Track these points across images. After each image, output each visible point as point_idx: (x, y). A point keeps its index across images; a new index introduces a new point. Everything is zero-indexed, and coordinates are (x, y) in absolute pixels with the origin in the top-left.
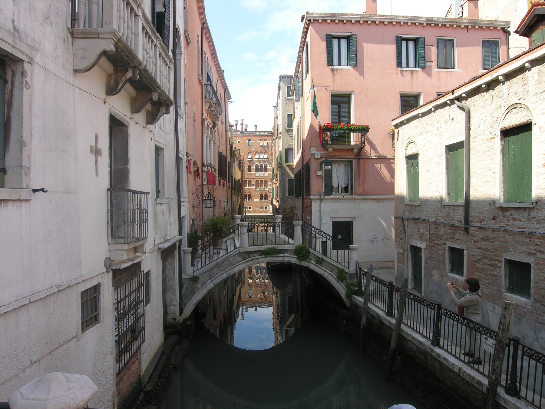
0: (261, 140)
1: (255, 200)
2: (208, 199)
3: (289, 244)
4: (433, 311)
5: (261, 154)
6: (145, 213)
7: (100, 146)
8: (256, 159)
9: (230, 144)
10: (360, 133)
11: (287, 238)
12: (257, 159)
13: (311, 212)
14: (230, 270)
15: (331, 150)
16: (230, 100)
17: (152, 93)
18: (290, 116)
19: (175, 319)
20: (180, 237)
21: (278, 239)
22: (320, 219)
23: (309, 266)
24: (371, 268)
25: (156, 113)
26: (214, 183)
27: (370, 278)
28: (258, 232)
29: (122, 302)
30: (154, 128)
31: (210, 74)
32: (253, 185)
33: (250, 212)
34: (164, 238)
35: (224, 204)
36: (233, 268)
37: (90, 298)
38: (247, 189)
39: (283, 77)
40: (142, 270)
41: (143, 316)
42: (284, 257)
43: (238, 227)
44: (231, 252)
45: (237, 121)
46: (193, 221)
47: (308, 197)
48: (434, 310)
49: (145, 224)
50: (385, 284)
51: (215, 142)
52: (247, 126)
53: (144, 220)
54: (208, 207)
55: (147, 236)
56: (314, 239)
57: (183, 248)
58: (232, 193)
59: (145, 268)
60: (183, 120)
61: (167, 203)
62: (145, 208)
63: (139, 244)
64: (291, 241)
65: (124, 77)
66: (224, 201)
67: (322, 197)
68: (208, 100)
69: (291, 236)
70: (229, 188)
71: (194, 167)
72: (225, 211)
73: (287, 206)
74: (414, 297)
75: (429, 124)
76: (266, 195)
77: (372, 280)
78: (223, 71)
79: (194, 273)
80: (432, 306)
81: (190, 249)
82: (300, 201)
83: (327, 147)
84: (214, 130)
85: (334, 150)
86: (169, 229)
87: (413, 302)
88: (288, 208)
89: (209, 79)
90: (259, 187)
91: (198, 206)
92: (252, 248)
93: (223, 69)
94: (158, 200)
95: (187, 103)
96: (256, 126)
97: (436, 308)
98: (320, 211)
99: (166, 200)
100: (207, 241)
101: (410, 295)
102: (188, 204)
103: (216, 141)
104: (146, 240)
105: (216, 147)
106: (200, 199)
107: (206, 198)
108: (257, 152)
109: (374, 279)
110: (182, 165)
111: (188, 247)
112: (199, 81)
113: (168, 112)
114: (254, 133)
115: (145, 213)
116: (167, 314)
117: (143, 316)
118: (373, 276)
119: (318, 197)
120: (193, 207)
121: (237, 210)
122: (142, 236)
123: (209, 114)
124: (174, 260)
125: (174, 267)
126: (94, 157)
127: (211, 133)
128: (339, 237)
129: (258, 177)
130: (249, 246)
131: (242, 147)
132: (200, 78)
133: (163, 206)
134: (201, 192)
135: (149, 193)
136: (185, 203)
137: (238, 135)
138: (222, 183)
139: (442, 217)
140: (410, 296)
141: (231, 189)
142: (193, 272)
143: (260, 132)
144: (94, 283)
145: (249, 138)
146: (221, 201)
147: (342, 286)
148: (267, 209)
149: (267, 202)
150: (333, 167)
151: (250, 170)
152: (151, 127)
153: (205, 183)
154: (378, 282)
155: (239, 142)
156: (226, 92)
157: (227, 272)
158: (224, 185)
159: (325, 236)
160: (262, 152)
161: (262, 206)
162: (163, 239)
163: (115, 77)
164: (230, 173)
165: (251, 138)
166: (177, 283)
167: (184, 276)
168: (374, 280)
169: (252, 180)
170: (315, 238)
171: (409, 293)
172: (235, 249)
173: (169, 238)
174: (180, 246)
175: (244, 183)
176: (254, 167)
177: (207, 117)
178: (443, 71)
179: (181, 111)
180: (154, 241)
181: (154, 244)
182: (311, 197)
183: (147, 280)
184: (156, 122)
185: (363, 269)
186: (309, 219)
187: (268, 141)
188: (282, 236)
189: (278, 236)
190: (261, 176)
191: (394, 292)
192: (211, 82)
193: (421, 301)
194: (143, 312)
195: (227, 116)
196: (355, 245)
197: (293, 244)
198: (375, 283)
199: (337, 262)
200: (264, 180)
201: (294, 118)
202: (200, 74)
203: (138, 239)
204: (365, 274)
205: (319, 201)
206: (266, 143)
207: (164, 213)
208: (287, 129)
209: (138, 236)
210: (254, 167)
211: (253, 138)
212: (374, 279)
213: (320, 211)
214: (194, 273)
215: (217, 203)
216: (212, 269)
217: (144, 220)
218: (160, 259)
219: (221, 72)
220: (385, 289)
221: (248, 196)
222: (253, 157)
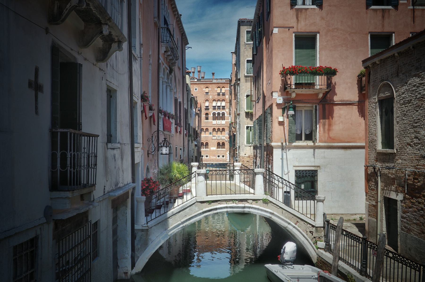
2: (164, 146)
4: (417, 273)
6: (93, 158)
7: (41, 81)
9: (187, 91)
10: (326, 77)
11: (247, 188)
16: (188, 46)
17: (102, 26)
19: (126, 273)
20: (133, 185)
21: (238, 189)
24: (341, 220)
25: (107, 50)
26: (170, 130)
27: (340, 232)
29: (64, 257)
30: (105, 67)
31: (167, 17)
32: (210, 133)
34: (116, 186)
35: (180, 152)
37: (25, 253)
38: (204, 137)
39: (242, 22)
40: (89, 221)
41: (89, 272)
43: (195, 175)
44: (187, 201)
48: (419, 271)
49: (93, 169)
50: (358, 239)
51: (171, 88)
53: (92, 165)
55: (95, 183)
57: (136, 196)
58: (189, 141)
59: (93, 219)
60: (138, 61)
61: (119, 148)
62: (93, 152)
63: (85, 191)
64: (252, 191)
65: (69, 4)
68: (164, 44)
69: (252, 185)
70: (186, 136)
72: (182, 158)
74: (393, 255)
75: (406, 64)
77: (342, 234)
78: (181, 15)
79: (147, 224)
80: (417, 266)
81: (144, 198)
83: (290, 92)
84: (171, 76)
86: (121, 176)
87: (392, 261)
89: (166, 22)
91: (153, 153)
92: (242, 196)
93: (180, 13)
94: (110, 145)
95: (142, 44)
96: (213, 74)
97: (422, 270)
99: (119, 145)
100: (162, 190)
101: (388, 253)
102: (143, 151)
104: (94, 187)
106: (156, 145)
107: (162, 145)
109: (344, 233)
110: (137, 109)
111: (142, 195)
112: (155, 24)
113: (120, 48)
115: (93, 158)
116: (118, 267)
117: (89, 272)
118: (343, 230)
120: (148, 154)
122: (90, 183)
123: (165, 59)
124: (127, 209)
125: (127, 216)
126: (34, 92)
127: (168, 78)
128: (303, 186)
129: (216, 125)
132: (156, 20)
133: (115, 151)
134: (157, 138)
135: (98, 136)
136: (139, 149)
137: (195, 83)
138: (179, 130)
139: (422, 166)
140: (388, 254)
141: (187, 137)
142: (147, 222)
144: (31, 235)
145: (206, 85)
146: (177, 148)
149: (224, 151)
151: (207, 118)
152: (102, 65)
153: (161, 128)
154: (349, 237)
155: (196, 89)
156: (183, 37)
158: (180, 132)
159: (285, 183)
162: (114, 187)
163: (59, 4)
165: (208, 85)
166: (129, 234)
167: (136, 227)
168: (345, 235)
169: (209, 128)
171: (387, 250)
172: (191, 199)
173: (121, 185)
174: (133, 195)
176: (211, 116)
177: (163, 62)
178: (419, 9)
179: (135, 52)
180: (104, 189)
181: (104, 192)
183: (95, 232)
184: (108, 59)
185: (331, 222)
188: (242, 185)
189: (238, 186)
191: (369, 249)
192: (167, 25)
193: (402, 260)
194: (89, 267)
197: (254, 194)
198: (345, 237)
199: (302, 214)
200: (221, 128)
202: (156, 15)
203: (85, 186)
204: (334, 227)
207: (116, 158)
208: (246, 75)
209: (85, 183)
210: (211, 116)
212: (344, 233)
214: (147, 224)
215: (173, 151)
217: (92, 165)
218: (111, 208)
219: (179, 16)
220: (355, 245)
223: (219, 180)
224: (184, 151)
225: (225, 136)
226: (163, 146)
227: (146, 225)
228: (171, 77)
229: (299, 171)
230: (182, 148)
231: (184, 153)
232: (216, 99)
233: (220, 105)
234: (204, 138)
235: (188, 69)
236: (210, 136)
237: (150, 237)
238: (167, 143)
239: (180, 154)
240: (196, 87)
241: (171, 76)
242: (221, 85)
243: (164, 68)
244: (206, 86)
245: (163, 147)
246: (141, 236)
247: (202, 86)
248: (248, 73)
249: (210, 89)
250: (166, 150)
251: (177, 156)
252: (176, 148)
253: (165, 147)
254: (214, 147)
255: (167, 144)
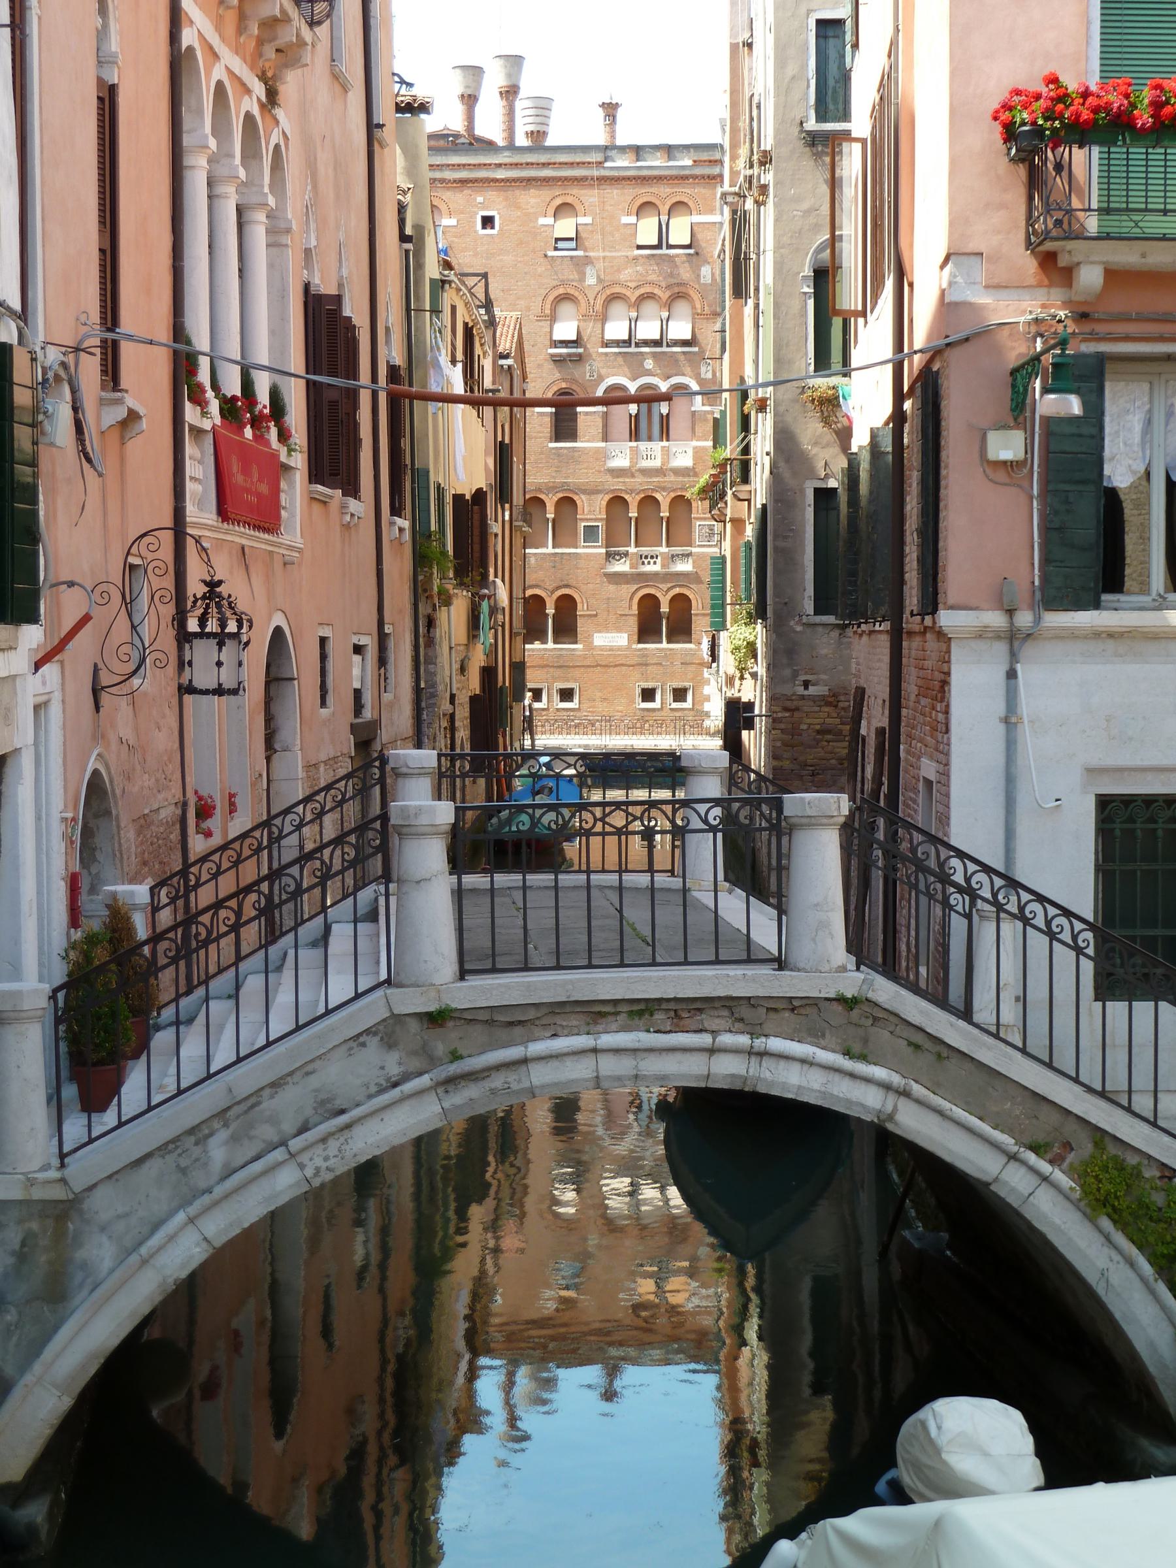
0: (645, 208)
1: (601, 640)
2: (202, 635)
3: (749, 960)
5: (650, 307)
8: (607, 344)
9: (404, 238)
12: (618, 343)
13: (947, 731)
14: (324, 1140)
15: (1090, 277)
18: (828, 28)
22: (1010, 780)
23: (891, 1117)
28: (588, 872)
32: (591, 532)
33: (568, 725)
35: (356, 671)
36: (348, 1126)
42: (712, 1051)
45: (474, 72)
46: (96, 788)
47: (928, 620)
52: (543, 107)
54: (206, 692)
56: (958, 924)
66: (358, 649)
67: (1024, 619)
71: (102, 402)
72: (368, 714)
73: (806, 684)
76: (681, 603)
79: (63, 1165)
82: (883, 644)
83: (1063, 261)
85: (1112, 275)
88: (814, 699)
90: (632, 549)
96: (610, 110)
98: (1010, 721)
103: (292, 213)
105: (292, 258)
108: (615, 298)
114: (598, 157)
119: (995, 619)
120: (96, 691)
121: (463, 714)
127: (251, 151)
130: (463, 974)
131: (508, 259)
142: (62, 1156)
143: (638, 151)
146: (330, 647)
147: (1132, 1264)
148: (688, 704)
150: (1111, 408)
157: (304, 1158)
160: (650, 296)
161: (650, 685)
164: (405, 443)
165: (573, 194)
169: (581, 500)
170: (968, 916)
175: (527, 517)
177: (214, 40)
182: (946, 619)
186: (932, 776)
187: (696, 218)
190: (645, 472)
195: (377, 35)
196: (548, 1105)
201: (856, 46)
205: (1002, 648)
206: (679, 232)
208: (812, 124)
211: (590, 197)
213: (1010, 721)
214: (63, 1165)
216: (198, 1133)
221: (550, 611)
222: (590, 329)
223: (580, 871)
224: (382, 661)
225: (694, 550)
226: (196, 635)
227: (54, 1174)
228: (277, 146)
229: (1127, 801)
230: (369, 641)
231: (383, 681)
232: (628, 293)
233: (657, 337)
234: (548, 564)
235: (410, 85)
236: (588, 555)
237: (80, 1255)
238: (228, 613)
239: (357, 685)
240: (483, 209)
241: (273, 141)
242: (664, 194)
243: (220, 85)
244: (558, 201)
245: (197, 642)
246: (23, 1244)
247: (533, 201)
248: (821, 117)
249: (588, 220)
250: (219, 664)
251: (330, 699)
252: (323, 641)
253: (213, 642)
254: (619, 630)
255: (223, 624)
